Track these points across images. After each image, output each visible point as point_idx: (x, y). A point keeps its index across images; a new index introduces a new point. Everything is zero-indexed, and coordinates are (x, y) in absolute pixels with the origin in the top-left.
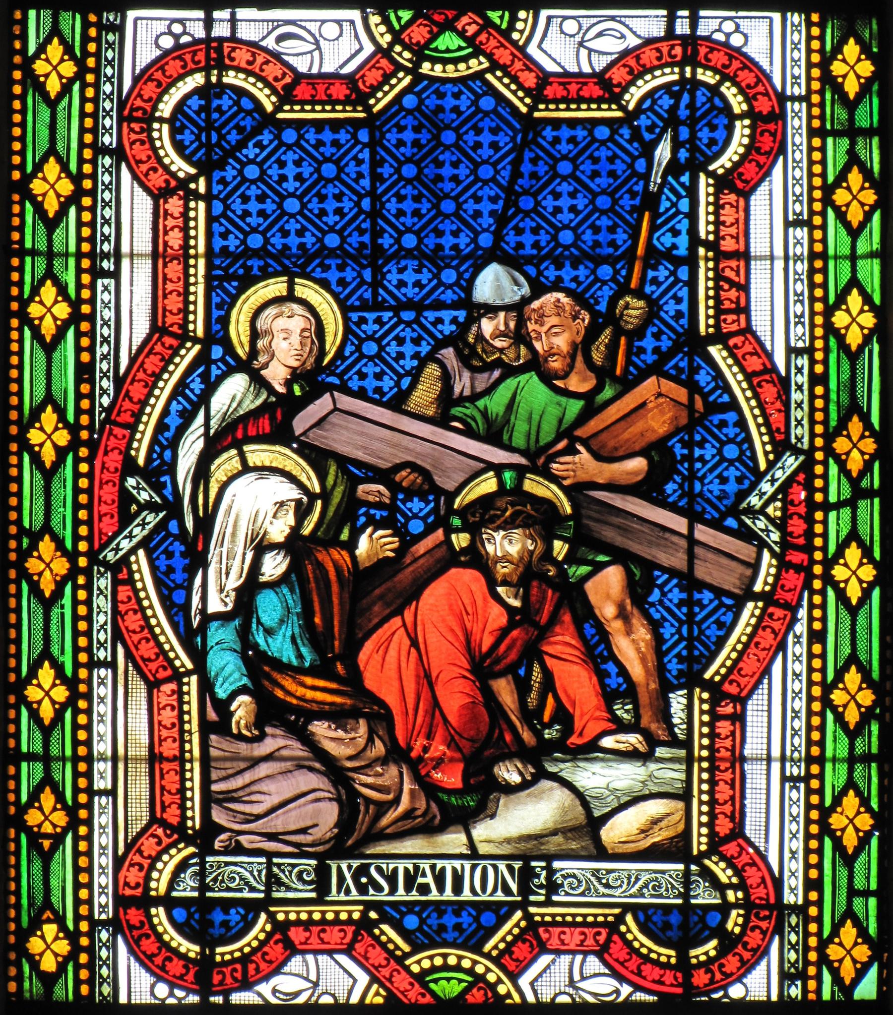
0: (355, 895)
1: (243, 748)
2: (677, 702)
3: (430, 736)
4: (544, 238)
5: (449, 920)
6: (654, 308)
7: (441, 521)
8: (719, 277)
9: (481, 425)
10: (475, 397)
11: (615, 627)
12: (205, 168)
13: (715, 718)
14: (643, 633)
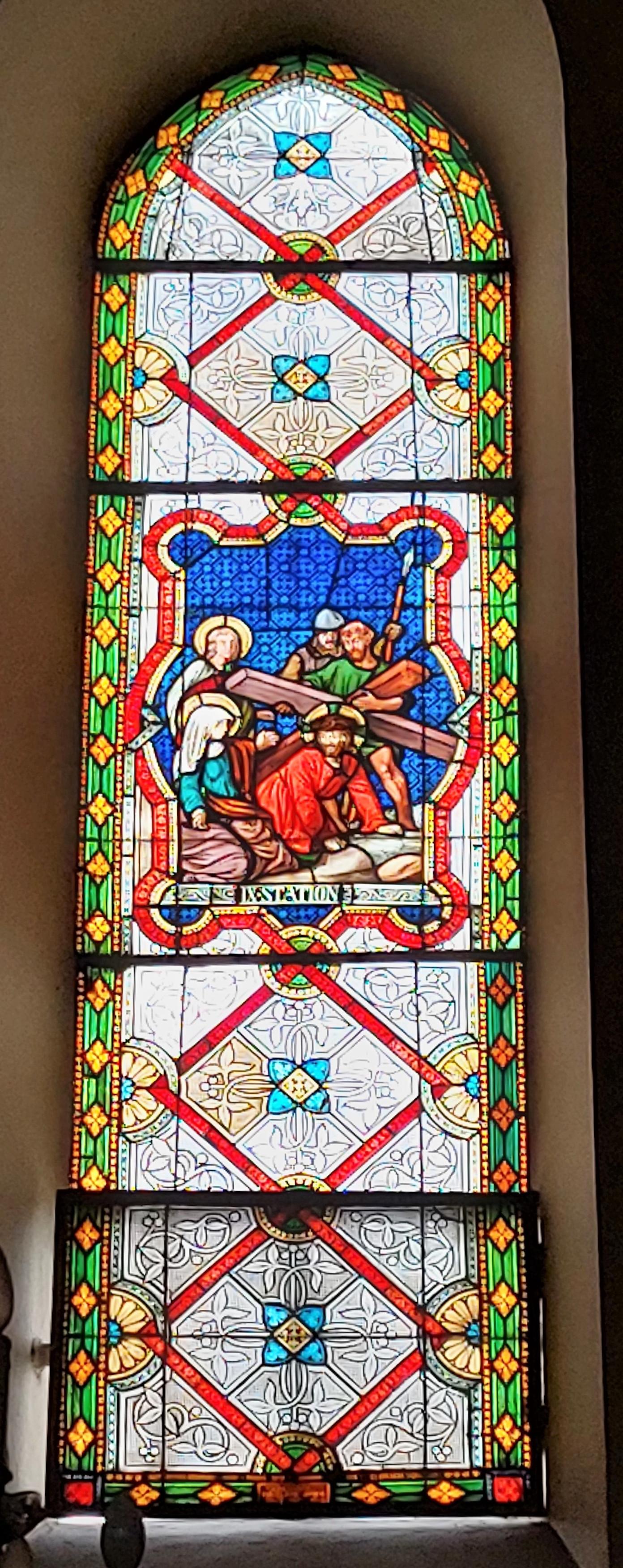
0: (255, 902)
1: (200, 835)
2: (417, 810)
3: (293, 828)
4: (351, 598)
5: (302, 913)
6: (404, 630)
7: (300, 728)
8: (437, 616)
9: (319, 683)
10: (316, 671)
11: (386, 776)
12: (185, 566)
13: (436, 818)
14: (400, 779)
